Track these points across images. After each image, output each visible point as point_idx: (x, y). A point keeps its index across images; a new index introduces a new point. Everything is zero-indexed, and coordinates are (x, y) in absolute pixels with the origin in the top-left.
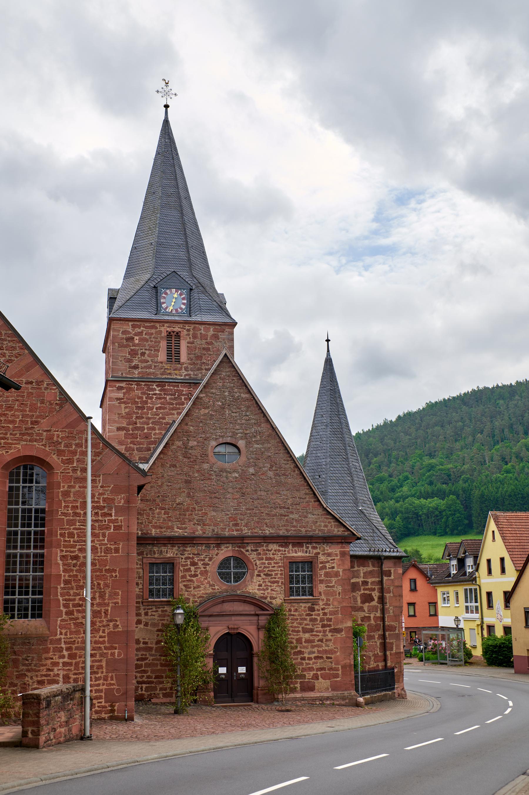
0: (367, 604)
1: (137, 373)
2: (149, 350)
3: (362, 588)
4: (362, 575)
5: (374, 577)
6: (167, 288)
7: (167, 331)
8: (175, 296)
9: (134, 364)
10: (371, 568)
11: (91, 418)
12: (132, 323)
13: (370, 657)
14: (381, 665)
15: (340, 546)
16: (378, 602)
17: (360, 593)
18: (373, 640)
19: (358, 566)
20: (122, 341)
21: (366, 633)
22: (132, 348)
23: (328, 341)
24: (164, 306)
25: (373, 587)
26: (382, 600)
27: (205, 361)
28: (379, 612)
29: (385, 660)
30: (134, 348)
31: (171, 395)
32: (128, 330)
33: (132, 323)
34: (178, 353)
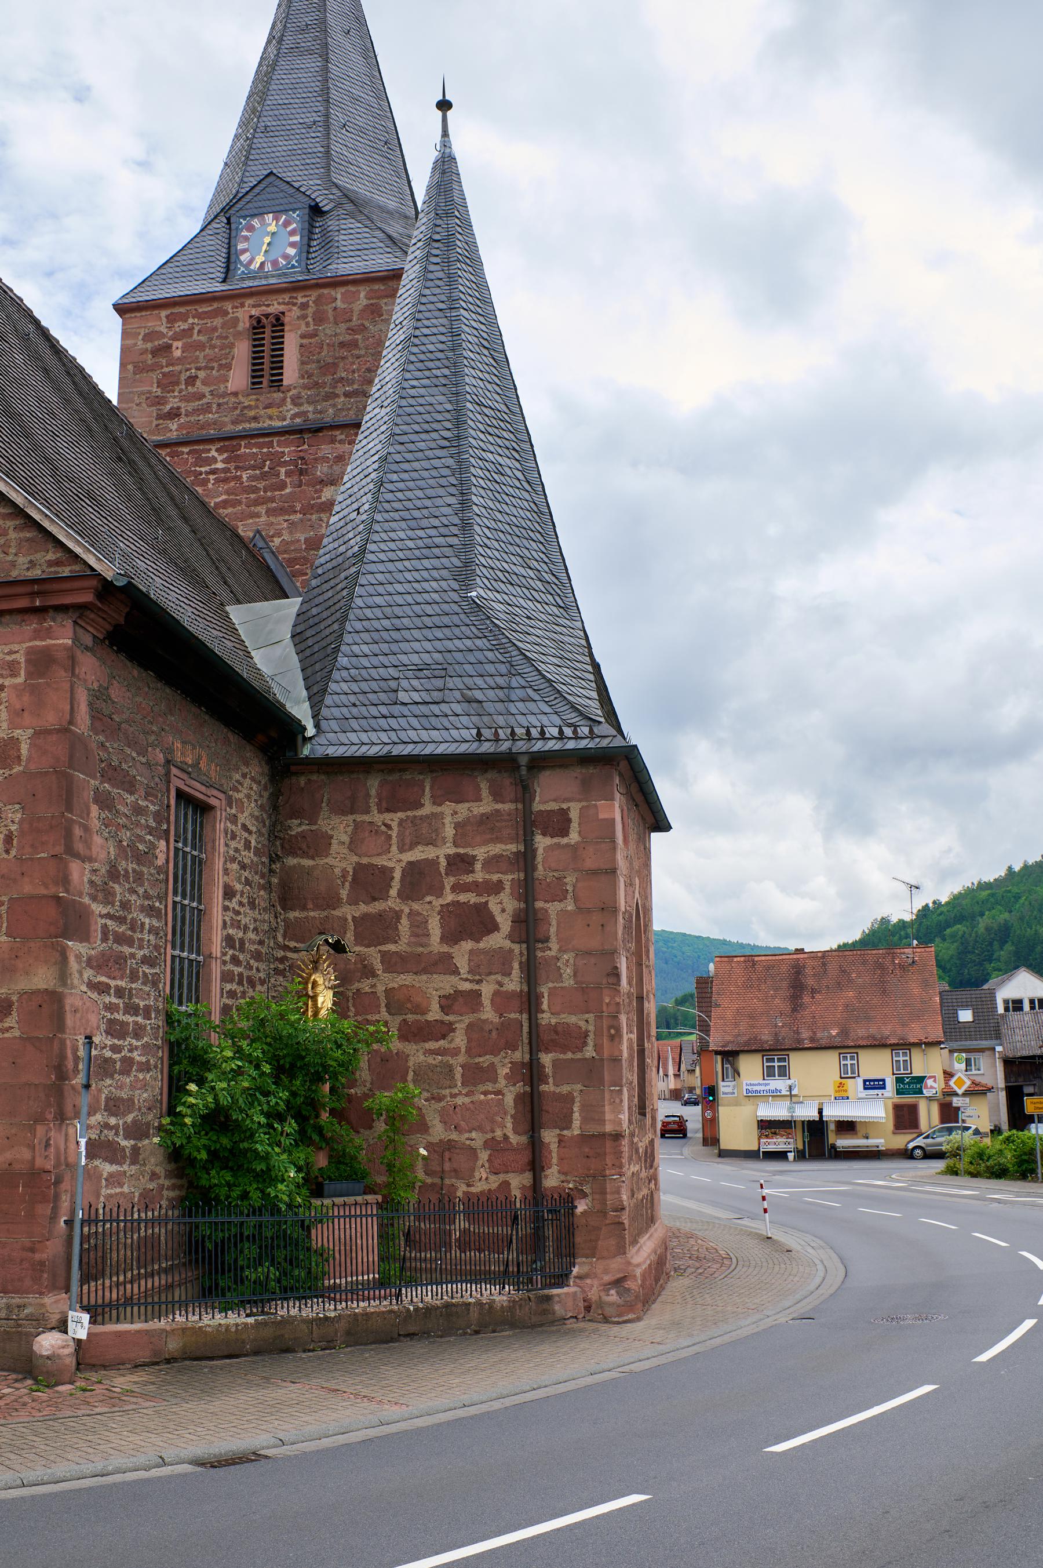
0: (468, 945)
1: (174, 427)
2: (206, 368)
3: (449, 882)
4: (449, 832)
5: (498, 840)
6: (253, 216)
7: (251, 317)
8: (272, 228)
9: (168, 407)
10: (485, 806)
11: (1010, 868)
12: (169, 312)
13: (473, 1152)
14: (518, 1182)
15: (31, 626)
16: (510, 937)
17: (438, 903)
18: (489, 1087)
19: (437, 801)
20: (144, 356)
21: (462, 1059)
22: (166, 370)
23: (444, 105)
24: (244, 258)
25: (495, 877)
26: (528, 927)
27: (344, 375)
28: (516, 971)
29: (536, 1165)
30: (171, 368)
31: (253, 468)
32: (157, 329)
33: (169, 312)
34: (278, 365)
